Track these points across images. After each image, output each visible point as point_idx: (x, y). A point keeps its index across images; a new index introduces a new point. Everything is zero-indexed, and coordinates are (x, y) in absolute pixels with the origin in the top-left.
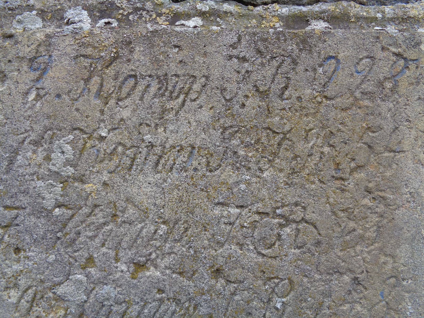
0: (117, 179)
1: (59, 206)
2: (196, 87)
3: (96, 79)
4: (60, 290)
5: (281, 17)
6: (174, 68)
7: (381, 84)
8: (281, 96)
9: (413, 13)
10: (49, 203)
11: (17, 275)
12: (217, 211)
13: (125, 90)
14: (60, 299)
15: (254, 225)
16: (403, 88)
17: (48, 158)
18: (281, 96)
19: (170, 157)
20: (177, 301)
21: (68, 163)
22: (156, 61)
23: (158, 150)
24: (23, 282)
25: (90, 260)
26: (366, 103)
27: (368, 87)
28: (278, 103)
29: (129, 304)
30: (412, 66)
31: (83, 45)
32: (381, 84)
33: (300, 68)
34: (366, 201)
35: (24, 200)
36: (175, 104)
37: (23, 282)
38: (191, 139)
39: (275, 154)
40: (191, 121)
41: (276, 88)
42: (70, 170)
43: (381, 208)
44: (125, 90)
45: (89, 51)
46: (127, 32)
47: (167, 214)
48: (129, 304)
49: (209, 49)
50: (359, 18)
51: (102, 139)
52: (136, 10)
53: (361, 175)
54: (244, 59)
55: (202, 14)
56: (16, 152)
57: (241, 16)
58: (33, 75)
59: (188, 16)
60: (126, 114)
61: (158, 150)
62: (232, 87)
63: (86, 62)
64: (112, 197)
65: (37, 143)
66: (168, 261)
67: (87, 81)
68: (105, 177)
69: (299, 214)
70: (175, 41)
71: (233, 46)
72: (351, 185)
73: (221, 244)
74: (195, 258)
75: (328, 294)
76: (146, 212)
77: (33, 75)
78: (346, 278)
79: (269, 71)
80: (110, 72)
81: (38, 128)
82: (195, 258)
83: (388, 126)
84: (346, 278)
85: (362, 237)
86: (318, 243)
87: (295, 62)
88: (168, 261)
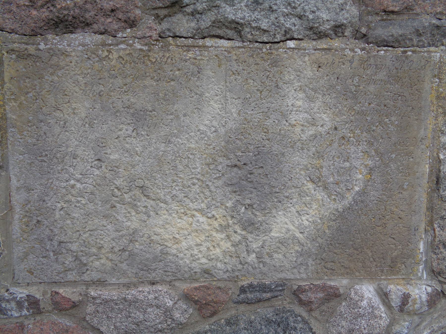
0: (366, 86)
1: (355, 91)
2: (383, 67)
3: (363, 65)
4: (354, 108)
5: (401, 51)
6: (378, 63)
7: (422, 67)
8: (400, 69)
9: (431, 50)
10: (353, 91)
11: (346, 105)
12: (386, 93)
13: (369, 68)
14: (354, 110)
15: (393, 96)
16: (426, 68)
17: (353, 81)
18: (400, 69)
19: (377, 82)
20: (377, 111)
21: (357, 82)
22: (375, 61)
23: (375, 80)
24: (347, 106)
25: (360, 102)
26: (418, 71)
27: (419, 67)
28: (400, 71)
29: (367, 111)
30: (429, 63)
31: (361, 58)
32: (422, 67)
33: (405, 63)
34: (416, 92)
35: (348, 90)
36: (378, 71)
37: (347, 106)
38: (382, 78)
39: (398, 82)
40: (156, 34)
41: (400, 68)
42: (357, 84)
43: (419, 94)
44: (369, 68)
45: (362, 59)
46: (369, 55)
47: (376, 94)
48: (367, 111)
49: (387, 59)
50: (418, 51)
51: (364, 78)
52: (370, 49)
53: (416, 87)
54: (393, 61)
55: (384, 50)
56: (346, 80)
57: (392, 51)
58: (350, 64)
59: (381, 51)
60: (369, 72)
61: (375, 80)
62: (390, 67)
63: (361, 61)
64: (365, 90)
65: (350, 78)
66: (375, 103)
67: (361, 65)
68: (364, 86)
69: (402, 94)
70: (379, 57)
71: (391, 58)
72: (413, 88)
73: (386, 100)
74: (381, 103)
75: (407, 111)
76: (372, 93)
77: (350, 64)
78: (411, 108)
79: (398, 64)
80: (366, 63)
81: (351, 75)
82: (381, 103)
83: (422, 76)
84: (411, 108)
85: (415, 100)
86: (406, 100)
87: (404, 62)
88: (375, 103)
